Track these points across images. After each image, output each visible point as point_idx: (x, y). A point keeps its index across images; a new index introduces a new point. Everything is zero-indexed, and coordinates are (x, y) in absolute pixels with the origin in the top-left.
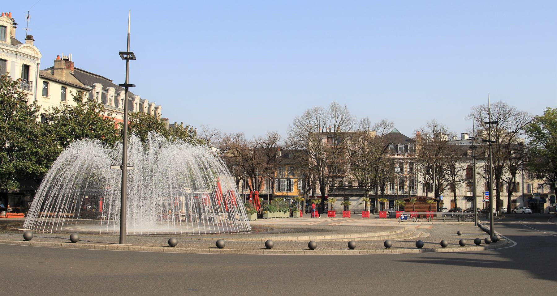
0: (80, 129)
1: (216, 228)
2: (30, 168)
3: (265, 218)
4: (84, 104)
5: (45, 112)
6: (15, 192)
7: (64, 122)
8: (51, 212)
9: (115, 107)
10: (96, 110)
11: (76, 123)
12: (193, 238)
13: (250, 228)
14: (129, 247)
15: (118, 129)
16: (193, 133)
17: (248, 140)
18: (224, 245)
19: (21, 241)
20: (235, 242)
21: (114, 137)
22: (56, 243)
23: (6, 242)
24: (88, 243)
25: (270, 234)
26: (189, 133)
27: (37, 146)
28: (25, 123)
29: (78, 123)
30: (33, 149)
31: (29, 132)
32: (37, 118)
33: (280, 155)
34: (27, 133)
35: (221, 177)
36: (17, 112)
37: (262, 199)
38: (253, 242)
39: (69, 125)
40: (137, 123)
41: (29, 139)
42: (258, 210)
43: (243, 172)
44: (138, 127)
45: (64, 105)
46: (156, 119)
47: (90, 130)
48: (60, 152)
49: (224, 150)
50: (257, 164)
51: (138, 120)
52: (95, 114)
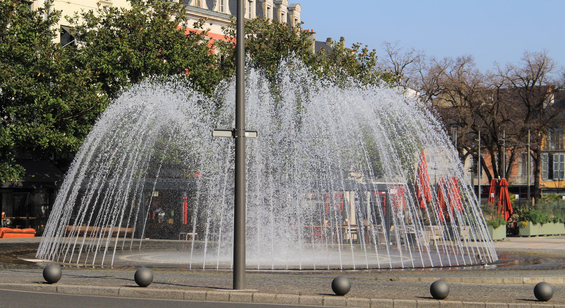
0: (140, 57)
1: (425, 257)
2: (45, 139)
3: (524, 236)
4: (146, 4)
5: (68, 24)
6: (14, 186)
7: (107, 43)
8: (122, 226)
9: (207, 8)
10: (170, 16)
11: (131, 45)
12: (380, 277)
13: (495, 258)
14: (252, 296)
15: (216, 55)
16: (367, 59)
17: (483, 72)
18: (448, 291)
19: (40, 285)
20: (466, 287)
21: (208, 72)
22: (108, 288)
23: (11, 287)
24: (170, 288)
25: (540, 269)
26: (360, 59)
27: (57, 93)
28: (31, 46)
29: (135, 44)
30: (49, 99)
31: (39, 65)
32: (55, 35)
33: (553, 102)
34: (36, 68)
35: (428, 151)
36: (14, 24)
37: (517, 196)
38: (505, 285)
39: (118, 48)
40: (252, 41)
41: (40, 79)
42: (508, 219)
43: (474, 139)
44: (256, 50)
45: (105, 7)
46: (293, 32)
47: (159, 57)
48: (102, 104)
49: (433, 94)
50: (504, 121)
51: (255, 36)
52: (169, 26)
